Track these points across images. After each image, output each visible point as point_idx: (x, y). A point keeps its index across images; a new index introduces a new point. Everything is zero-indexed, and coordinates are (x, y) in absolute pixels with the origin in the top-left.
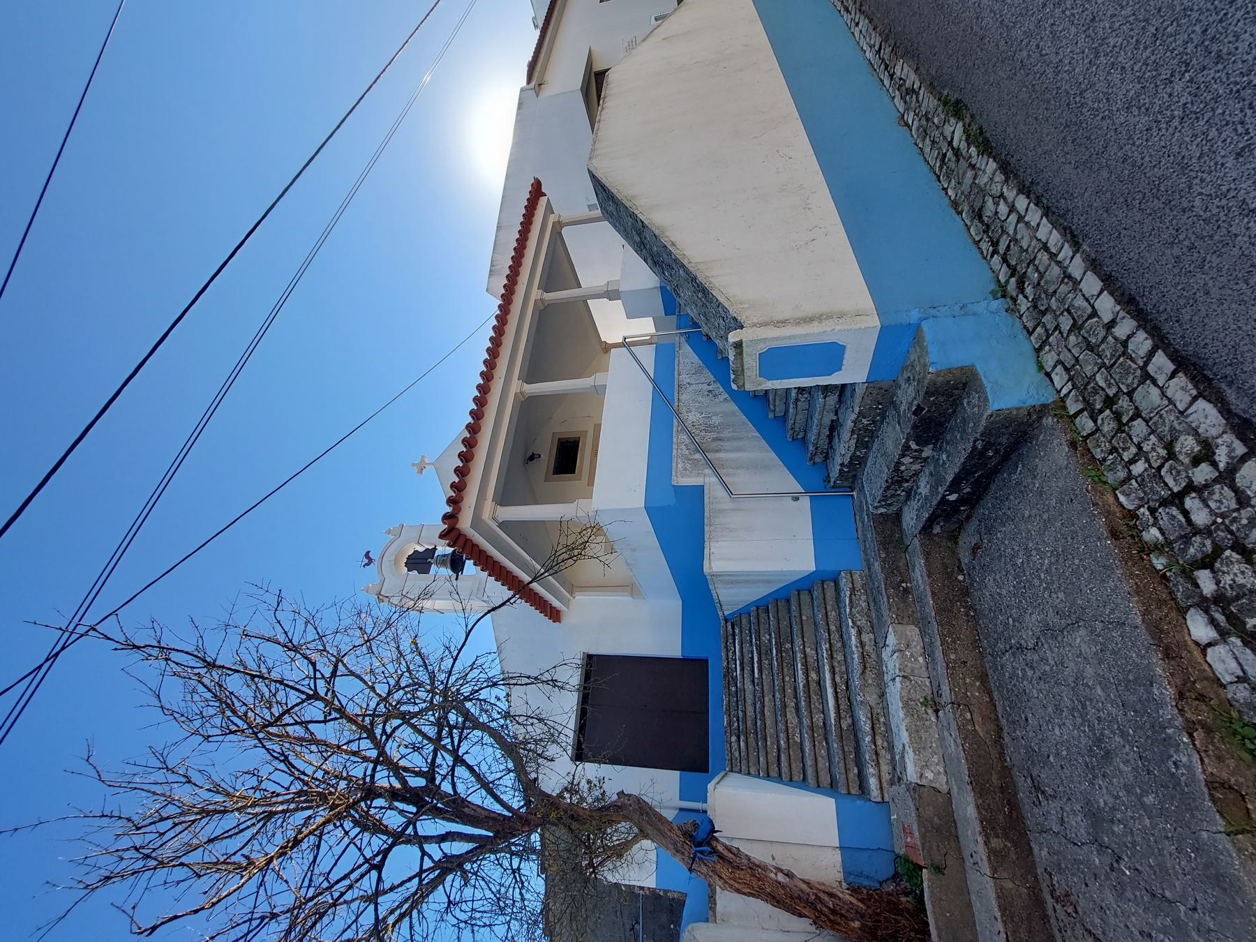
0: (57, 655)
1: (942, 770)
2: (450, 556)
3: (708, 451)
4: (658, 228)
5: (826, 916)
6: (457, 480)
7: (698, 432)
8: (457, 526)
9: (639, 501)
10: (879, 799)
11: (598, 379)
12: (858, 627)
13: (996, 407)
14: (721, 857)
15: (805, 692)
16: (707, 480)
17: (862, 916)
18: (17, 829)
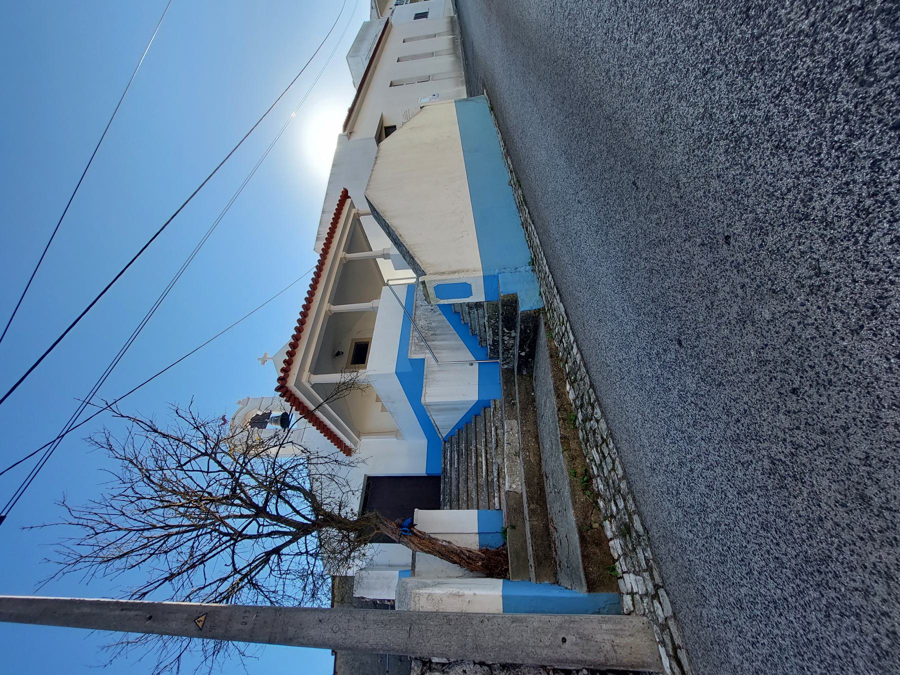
0: (63, 436)
1: (520, 484)
2: (280, 418)
3: (428, 341)
4: (395, 227)
5: (465, 560)
6: (287, 358)
7: (424, 331)
8: (286, 385)
9: (392, 369)
10: (498, 508)
11: (374, 303)
12: (496, 427)
13: (522, 310)
14: (416, 535)
15: (475, 467)
16: (427, 355)
17: (483, 560)
18: (32, 528)
